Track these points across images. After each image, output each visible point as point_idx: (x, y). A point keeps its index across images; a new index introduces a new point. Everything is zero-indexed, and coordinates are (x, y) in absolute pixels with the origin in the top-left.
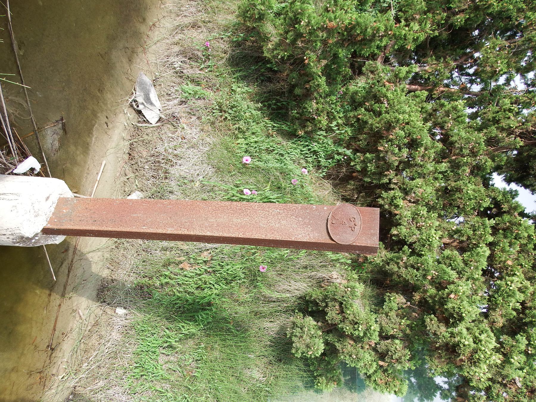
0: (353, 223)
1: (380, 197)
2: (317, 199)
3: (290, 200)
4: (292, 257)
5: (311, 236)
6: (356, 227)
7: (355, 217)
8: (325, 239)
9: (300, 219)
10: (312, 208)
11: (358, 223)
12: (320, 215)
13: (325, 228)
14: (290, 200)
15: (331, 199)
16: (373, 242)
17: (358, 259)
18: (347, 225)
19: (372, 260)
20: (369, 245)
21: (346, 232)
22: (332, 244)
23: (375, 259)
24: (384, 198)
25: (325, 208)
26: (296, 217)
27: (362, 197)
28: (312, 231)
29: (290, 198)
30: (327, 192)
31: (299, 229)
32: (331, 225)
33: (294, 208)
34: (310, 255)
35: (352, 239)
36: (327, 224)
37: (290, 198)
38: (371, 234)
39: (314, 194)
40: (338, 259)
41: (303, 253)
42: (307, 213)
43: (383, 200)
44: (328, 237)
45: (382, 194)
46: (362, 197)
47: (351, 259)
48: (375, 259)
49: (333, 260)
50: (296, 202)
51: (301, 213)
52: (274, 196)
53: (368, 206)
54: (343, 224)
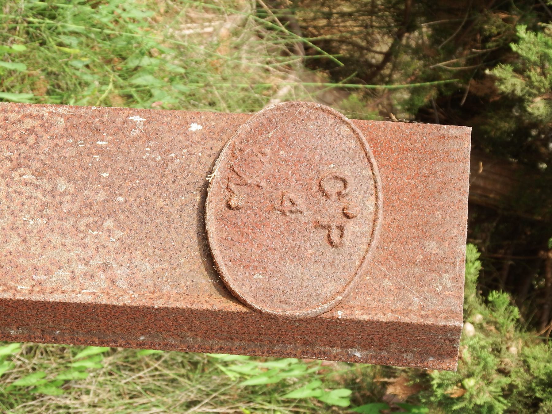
0: (333, 209)
1: (502, 54)
2: (174, 66)
3: (21, 67)
4: (32, 380)
5: (120, 272)
6: (350, 227)
7: (347, 173)
8: (186, 289)
9: (62, 185)
10: (125, 128)
11: (362, 202)
12: (167, 162)
13: (193, 232)
14: (21, 67)
15: (251, 62)
16: (434, 304)
17: (385, 385)
18: (307, 216)
19: (453, 391)
20: (414, 319)
21: (297, 255)
22: (226, 316)
23: (470, 383)
24: (526, 61)
25: (194, 127)
26: (40, 174)
27: (417, 52)
28: (125, 247)
29: (23, 57)
30: (229, 25)
31: (56, 239)
32: (221, 219)
33: (29, 123)
34: (131, 365)
35: (331, 287)
36: (202, 211)
37: (23, 57)
38: (427, 260)
39: (152, 40)
40: (282, 387)
41: (90, 360)
42: (100, 151)
43: (520, 71)
44: (205, 281)
45: (517, 40)
46: (417, 52)
47: (350, 384)
48: (470, 383)
49: (253, 391)
50: (59, 88)
51: (70, 152)
52: (527, 61)
53: (423, 115)
54: (284, 209)
